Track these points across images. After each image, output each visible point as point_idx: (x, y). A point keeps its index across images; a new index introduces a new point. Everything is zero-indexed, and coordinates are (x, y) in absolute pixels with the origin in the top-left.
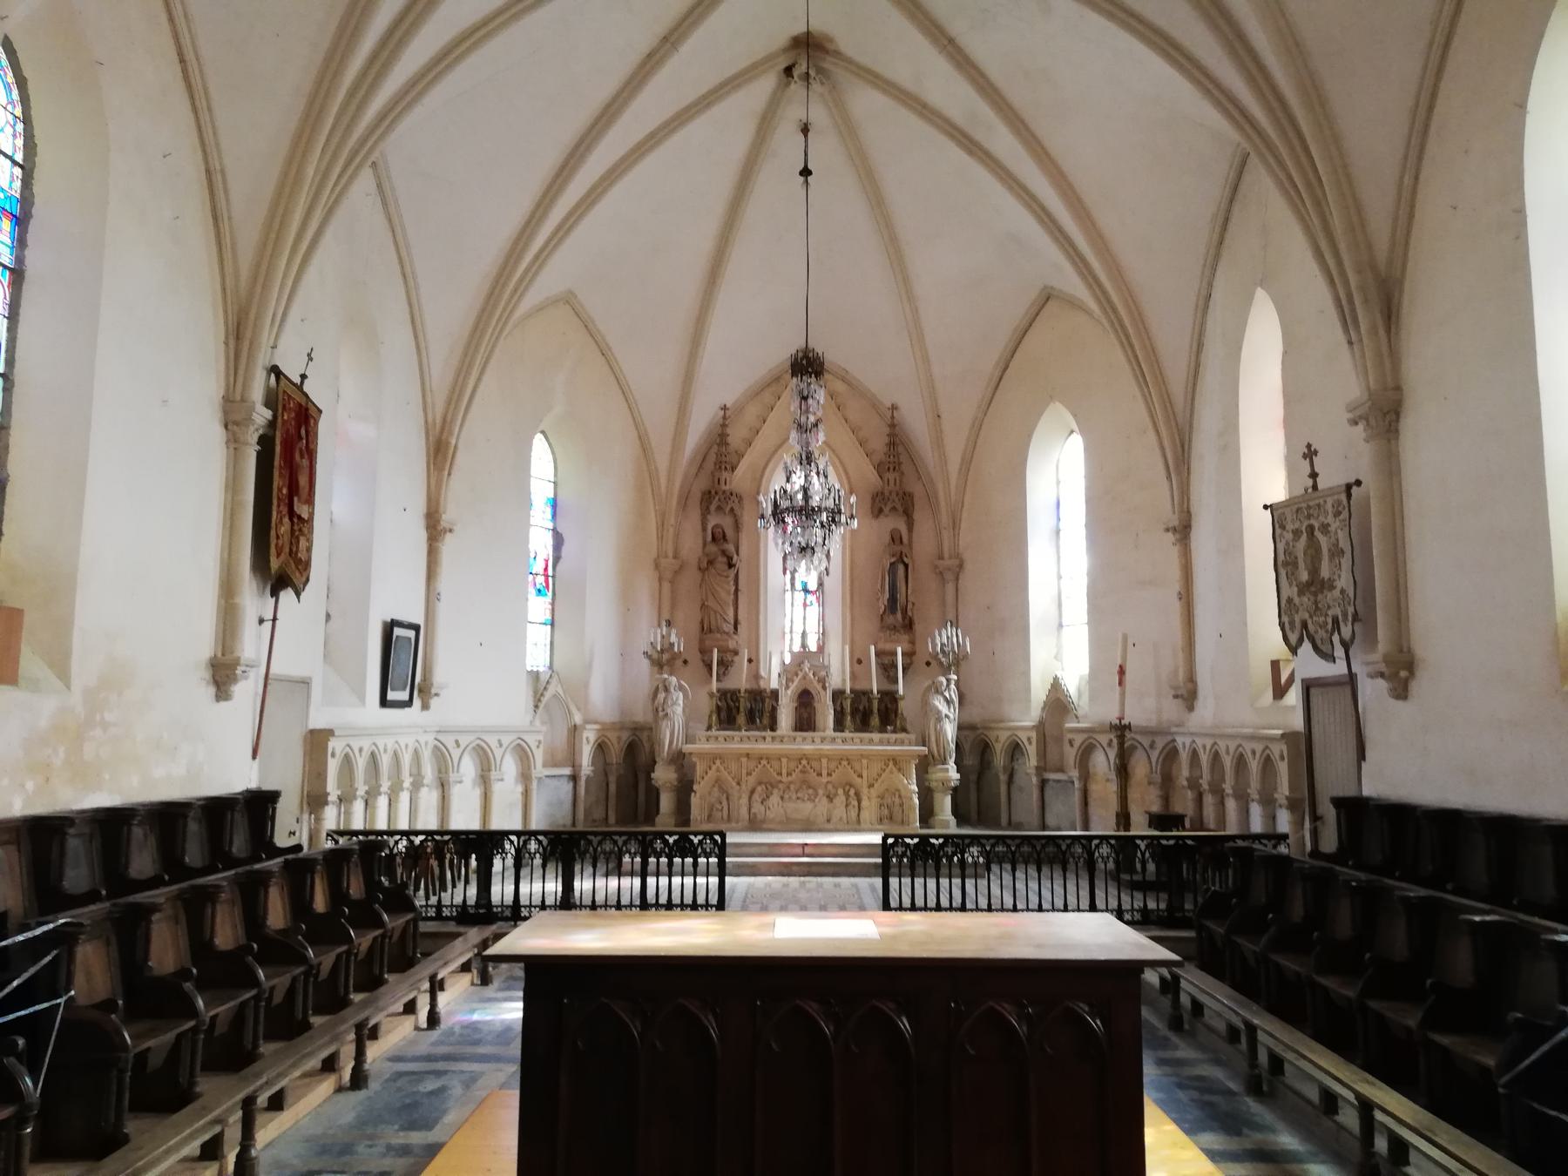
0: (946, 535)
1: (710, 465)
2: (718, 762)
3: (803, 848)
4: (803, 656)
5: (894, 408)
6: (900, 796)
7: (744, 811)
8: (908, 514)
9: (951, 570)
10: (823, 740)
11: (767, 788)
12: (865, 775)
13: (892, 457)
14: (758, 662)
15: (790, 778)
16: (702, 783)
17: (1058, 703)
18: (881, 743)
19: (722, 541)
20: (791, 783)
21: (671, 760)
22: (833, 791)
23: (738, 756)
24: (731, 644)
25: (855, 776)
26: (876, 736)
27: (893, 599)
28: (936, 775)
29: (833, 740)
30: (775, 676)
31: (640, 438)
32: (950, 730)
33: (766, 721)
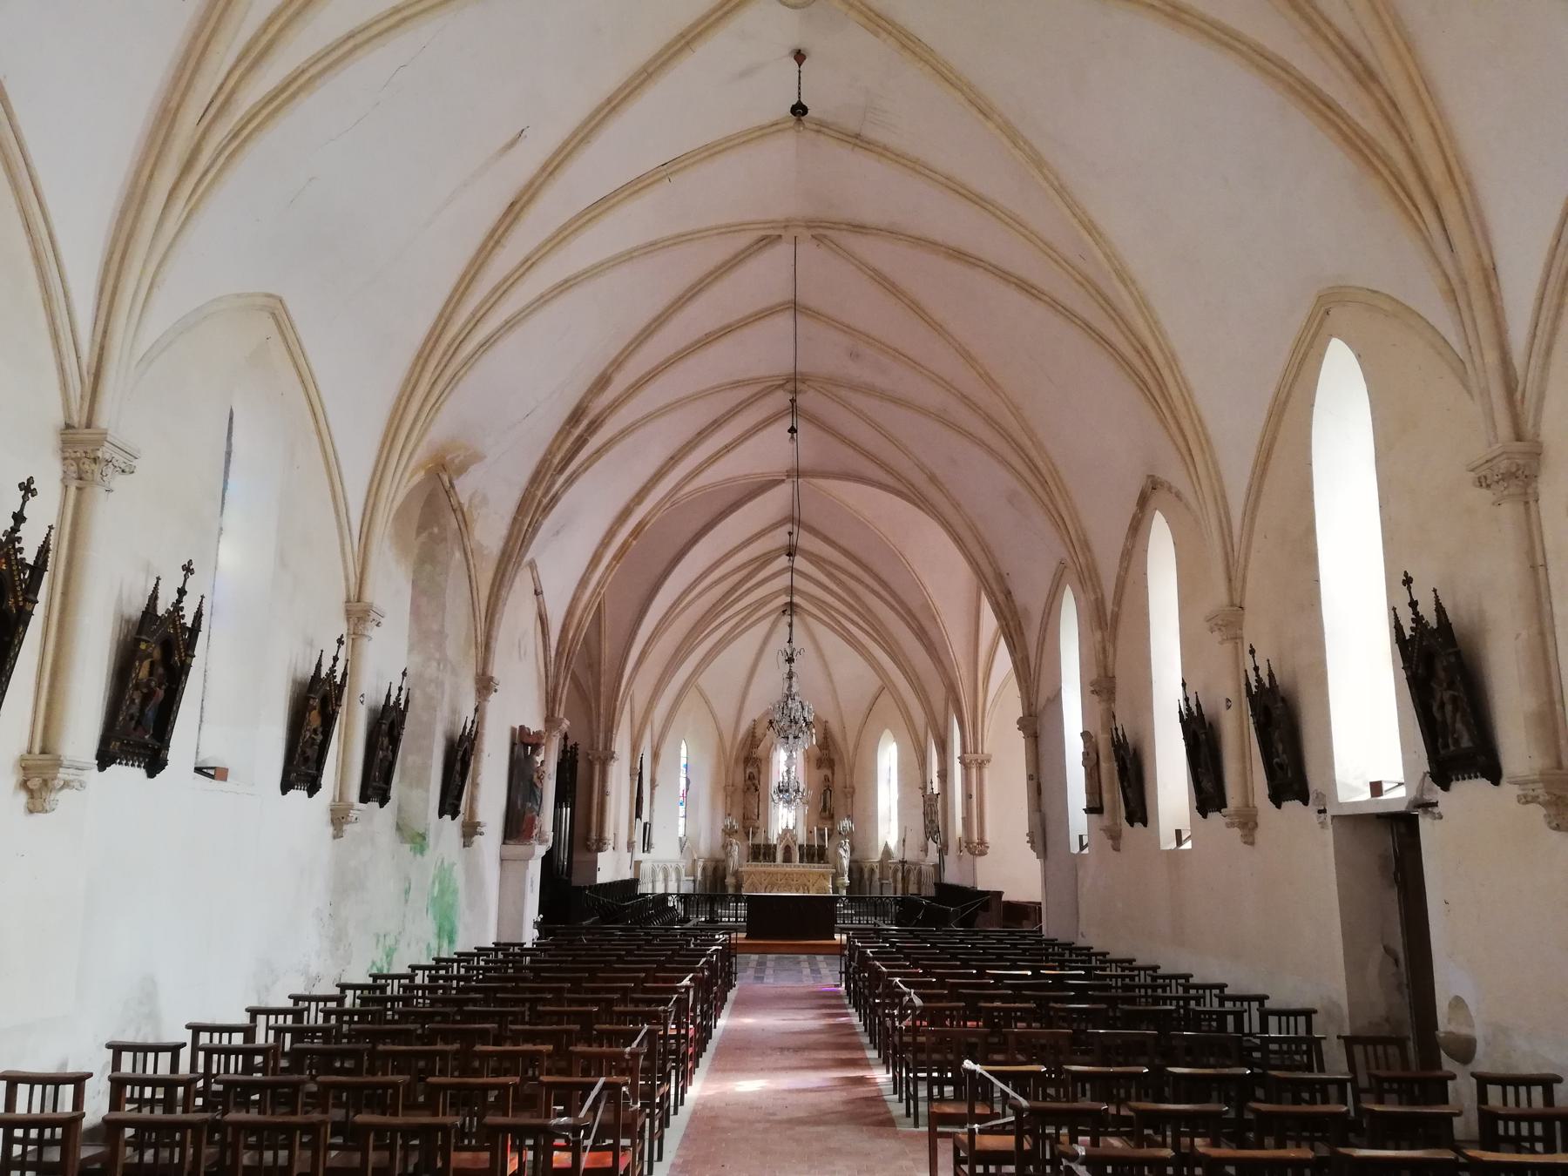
4: (786, 831)
5: (826, 722)
9: (850, 792)
17: (887, 852)
23: (760, 873)
24: (756, 825)
26: (816, 865)
28: (840, 881)
32: (846, 863)
33: (771, 857)
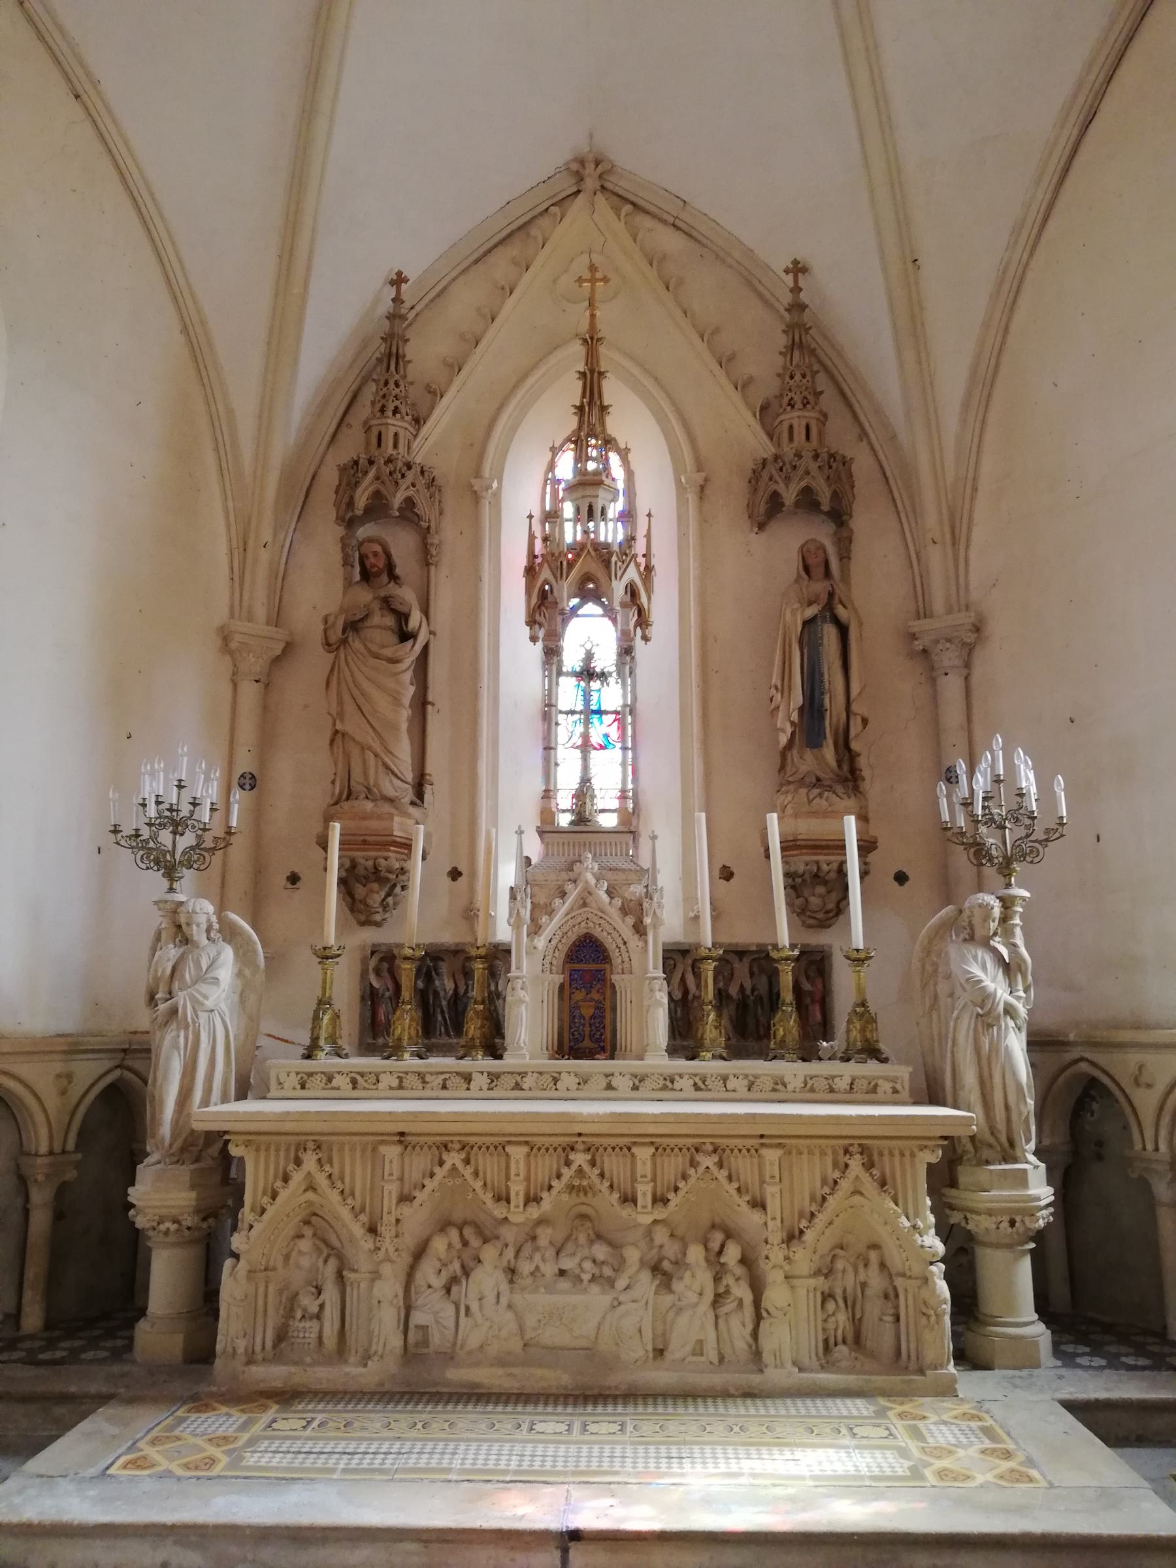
0: (936, 558)
1: (363, 410)
2: (310, 1161)
3: (565, 1551)
6: (883, 1265)
7: (387, 1321)
8: (839, 517)
10: (638, 1082)
11: (465, 1243)
12: (773, 1205)
13: (798, 377)
14: (473, 874)
15: (534, 1212)
16: (258, 1227)
18: (809, 1092)
19: (385, 578)
20: (540, 1222)
21: (183, 1150)
22: (671, 1250)
25: (742, 1202)
26: (793, 1070)
27: (812, 710)
29: (669, 1083)
30: (502, 908)
31: (185, 330)
